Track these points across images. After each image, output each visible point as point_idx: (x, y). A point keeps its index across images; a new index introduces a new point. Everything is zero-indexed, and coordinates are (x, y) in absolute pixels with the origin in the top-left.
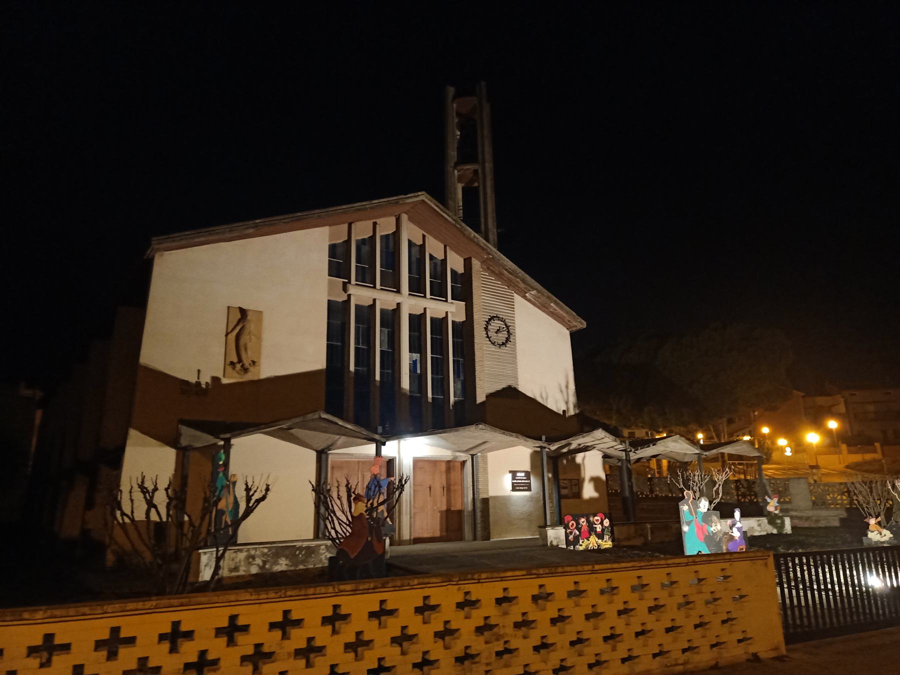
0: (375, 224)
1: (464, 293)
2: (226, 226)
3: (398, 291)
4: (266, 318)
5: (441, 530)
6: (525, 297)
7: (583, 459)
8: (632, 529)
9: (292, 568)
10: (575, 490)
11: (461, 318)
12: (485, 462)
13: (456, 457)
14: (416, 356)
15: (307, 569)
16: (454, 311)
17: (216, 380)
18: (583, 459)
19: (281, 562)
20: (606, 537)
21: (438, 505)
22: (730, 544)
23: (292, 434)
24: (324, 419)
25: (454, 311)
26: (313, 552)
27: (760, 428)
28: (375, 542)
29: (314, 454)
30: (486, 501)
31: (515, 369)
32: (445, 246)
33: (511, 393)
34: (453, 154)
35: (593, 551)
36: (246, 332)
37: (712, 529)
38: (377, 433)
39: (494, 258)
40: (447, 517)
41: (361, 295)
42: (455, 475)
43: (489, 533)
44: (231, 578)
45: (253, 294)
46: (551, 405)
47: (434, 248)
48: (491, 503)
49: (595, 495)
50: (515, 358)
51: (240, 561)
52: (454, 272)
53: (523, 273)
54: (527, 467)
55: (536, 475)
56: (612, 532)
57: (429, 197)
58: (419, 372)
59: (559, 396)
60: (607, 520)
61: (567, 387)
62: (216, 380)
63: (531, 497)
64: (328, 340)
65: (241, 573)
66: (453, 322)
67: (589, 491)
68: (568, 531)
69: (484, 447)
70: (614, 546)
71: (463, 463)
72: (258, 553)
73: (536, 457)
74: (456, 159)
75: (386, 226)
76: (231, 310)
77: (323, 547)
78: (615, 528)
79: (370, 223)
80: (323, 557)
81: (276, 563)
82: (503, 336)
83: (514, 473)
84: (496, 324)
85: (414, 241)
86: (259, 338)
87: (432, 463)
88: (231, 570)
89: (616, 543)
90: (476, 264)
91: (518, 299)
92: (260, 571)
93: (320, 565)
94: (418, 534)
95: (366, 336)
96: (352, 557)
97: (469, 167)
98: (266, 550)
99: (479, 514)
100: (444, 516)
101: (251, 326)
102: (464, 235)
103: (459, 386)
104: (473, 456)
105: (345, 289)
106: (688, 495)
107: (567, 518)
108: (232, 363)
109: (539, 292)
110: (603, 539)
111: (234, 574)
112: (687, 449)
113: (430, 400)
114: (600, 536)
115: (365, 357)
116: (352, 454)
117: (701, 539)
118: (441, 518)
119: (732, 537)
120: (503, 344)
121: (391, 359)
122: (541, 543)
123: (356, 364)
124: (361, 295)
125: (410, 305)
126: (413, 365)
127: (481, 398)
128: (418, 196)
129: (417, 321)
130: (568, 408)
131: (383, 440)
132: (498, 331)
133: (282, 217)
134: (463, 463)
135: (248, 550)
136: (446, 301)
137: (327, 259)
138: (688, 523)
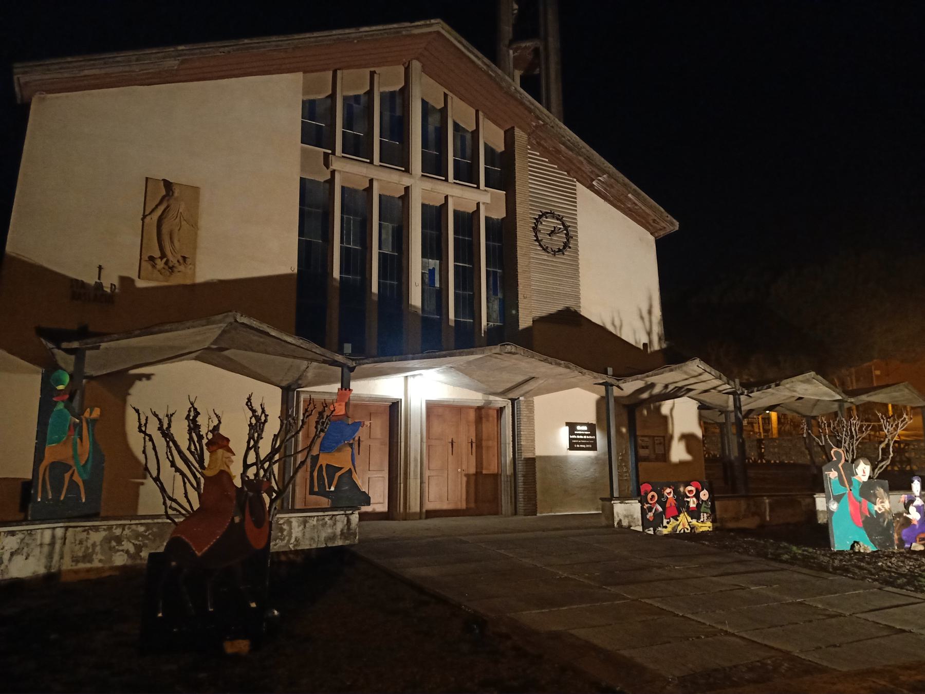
0: (372, 74)
1: (503, 176)
2: (131, 53)
3: (407, 171)
4: (205, 198)
6: (591, 187)
7: (672, 410)
8: (743, 504)
10: (660, 450)
11: (499, 214)
12: (531, 409)
13: (490, 402)
14: (434, 263)
16: (485, 201)
18: (672, 410)
20: (704, 516)
21: (464, 467)
22: (905, 531)
24: (243, 324)
25: (485, 201)
28: (249, 526)
29: (279, 391)
30: (531, 462)
31: (576, 286)
32: (477, 112)
33: (570, 318)
34: (507, 29)
35: (683, 536)
37: (876, 508)
38: (342, 354)
39: (545, 124)
41: (350, 172)
42: (488, 428)
43: (535, 505)
44: (76, 572)
46: (627, 335)
47: (461, 113)
48: (537, 464)
49: (687, 457)
50: (577, 270)
51: (94, 545)
52: (489, 151)
53: (588, 147)
54: (592, 419)
55: (602, 429)
56: (713, 509)
57: (447, 27)
58: (437, 285)
59: (638, 324)
60: (705, 491)
61: (650, 312)
63: (597, 459)
64: (301, 233)
65: (96, 564)
66: (487, 219)
67: (678, 453)
68: (646, 506)
69: (526, 388)
70: (715, 529)
71: (501, 410)
73: (602, 405)
74: (511, 36)
75: (389, 80)
76: (149, 181)
78: (716, 503)
79: (367, 71)
83: (572, 426)
84: (548, 224)
85: (431, 102)
87: (455, 410)
88: (76, 560)
89: (718, 525)
90: (520, 136)
91: (580, 188)
92: (129, 562)
94: (429, 506)
96: (199, 554)
97: (528, 44)
98: (141, 529)
99: (520, 479)
100: (473, 479)
102: (501, 88)
103: (496, 306)
104: (513, 401)
105: (327, 164)
107: (645, 487)
108: (151, 259)
109: (610, 176)
110: (698, 518)
111: (81, 566)
112: (826, 394)
113: (452, 324)
114: (695, 514)
115: (356, 261)
117: (857, 524)
118: (468, 483)
119: (908, 521)
121: (395, 266)
122: (603, 521)
125: (423, 190)
126: (428, 278)
127: (525, 322)
129: (434, 216)
130: (651, 341)
131: (351, 364)
132: (552, 233)
133: (218, 44)
134: (501, 410)
135: (110, 528)
136: (478, 188)
137: (300, 119)
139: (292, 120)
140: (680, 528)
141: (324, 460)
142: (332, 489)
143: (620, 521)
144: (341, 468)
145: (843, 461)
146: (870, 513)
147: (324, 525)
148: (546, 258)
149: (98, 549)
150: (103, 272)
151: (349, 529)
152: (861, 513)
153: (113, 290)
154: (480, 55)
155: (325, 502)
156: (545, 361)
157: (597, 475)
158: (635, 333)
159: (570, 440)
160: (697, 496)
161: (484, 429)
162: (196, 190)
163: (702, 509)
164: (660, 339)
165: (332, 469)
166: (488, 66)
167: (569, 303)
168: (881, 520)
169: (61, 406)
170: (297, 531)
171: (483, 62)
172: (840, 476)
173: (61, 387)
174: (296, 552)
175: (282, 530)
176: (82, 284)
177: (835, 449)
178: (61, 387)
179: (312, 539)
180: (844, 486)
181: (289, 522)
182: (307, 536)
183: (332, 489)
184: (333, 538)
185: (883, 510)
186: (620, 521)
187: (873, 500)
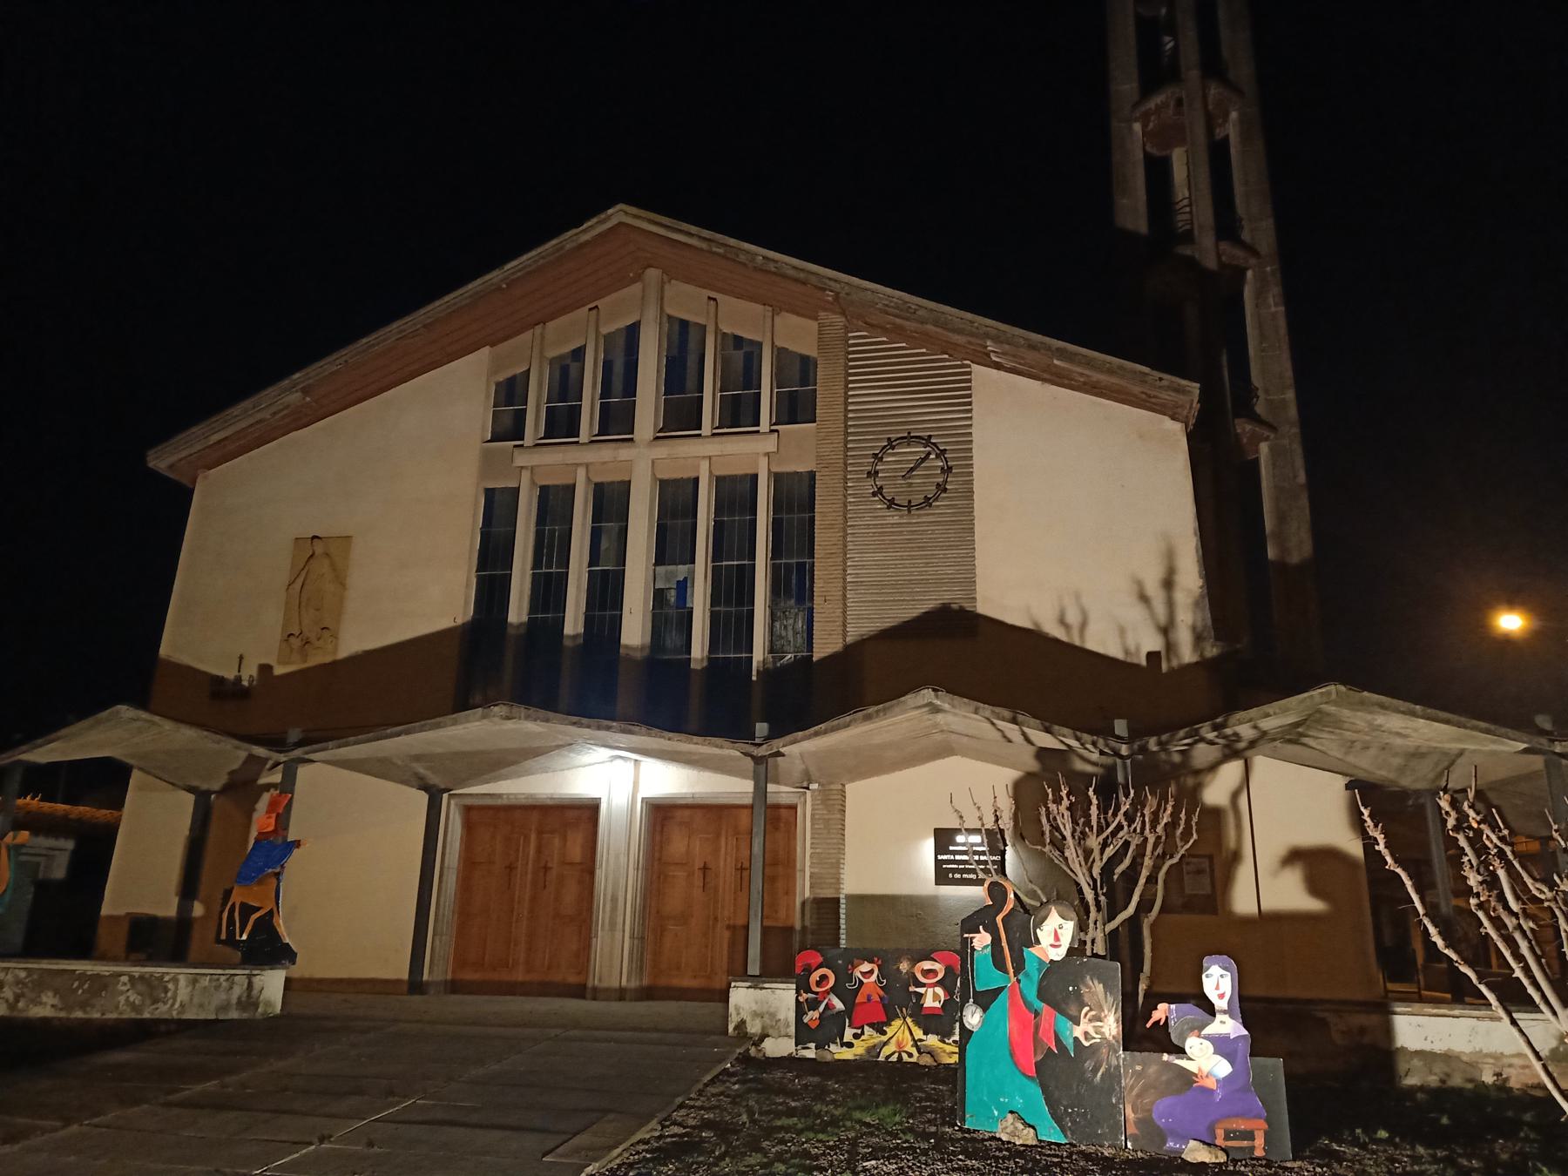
9: (62, 1014)
16: (757, 453)
17: (265, 669)
19: (44, 999)
23: (1013, 767)
26: (105, 987)
27: (1535, 624)
41: (538, 463)
46: (1101, 641)
50: (972, 531)
59: (1134, 614)
61: (1168, 584)
62: (265, 669)
77: (124, 979)
81: (37, 1002)
82: (923, 483)
83: (943, 838)
86: (341, 581)
93: (114, 1016)
95: (552, 547)
115: (549, 591)
116: (500, 796)
121: (606, 592)
128: (609, 218)
130: (1170, 646)
140: (886, 1051)
141: (237, 897)
142: (244, 937)
143: (743, 1022)
147: (217, 988)
148: (896, 520)
151: (249, 996)
152: (1037, 1041)
153: (251, 682)
154: (694, 229)
156: (580, 725)
159: (938, 863)
164: (1198, 638)
165: (247, 910)
168: (1089, 1065)
170: (183, 992)
172: (996, 942)
175: (166, 990)
176: (220, 680)
179: (201, 1006)
181: (175, 980)
183: (244, 937)
184: (225, 1007)
186: (743, 1022)
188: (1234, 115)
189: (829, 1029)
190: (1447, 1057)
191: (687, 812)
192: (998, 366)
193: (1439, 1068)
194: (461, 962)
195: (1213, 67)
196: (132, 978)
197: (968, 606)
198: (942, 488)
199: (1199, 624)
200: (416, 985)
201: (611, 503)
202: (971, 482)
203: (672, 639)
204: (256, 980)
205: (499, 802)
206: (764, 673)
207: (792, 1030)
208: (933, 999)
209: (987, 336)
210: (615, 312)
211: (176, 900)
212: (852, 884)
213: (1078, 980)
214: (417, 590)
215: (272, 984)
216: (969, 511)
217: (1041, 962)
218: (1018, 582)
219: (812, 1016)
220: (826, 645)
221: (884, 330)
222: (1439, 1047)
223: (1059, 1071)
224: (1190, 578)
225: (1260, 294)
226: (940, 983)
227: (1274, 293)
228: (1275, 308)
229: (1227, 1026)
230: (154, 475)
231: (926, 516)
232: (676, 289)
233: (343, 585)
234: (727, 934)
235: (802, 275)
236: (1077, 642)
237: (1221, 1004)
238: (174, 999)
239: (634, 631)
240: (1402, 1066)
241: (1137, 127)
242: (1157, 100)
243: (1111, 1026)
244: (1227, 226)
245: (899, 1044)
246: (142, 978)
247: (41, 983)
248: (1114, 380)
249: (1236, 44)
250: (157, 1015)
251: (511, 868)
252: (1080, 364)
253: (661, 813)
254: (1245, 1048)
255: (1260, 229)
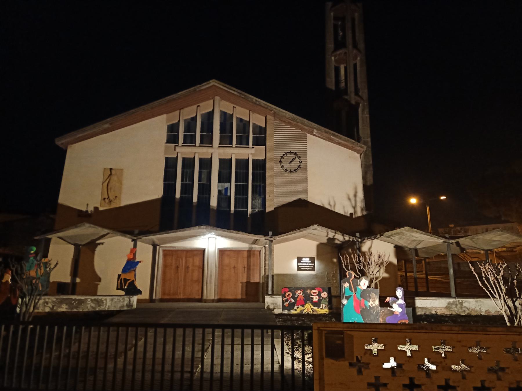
1: (261, 140)
5: (242, 294)
9: (69, 310)
15: (78, 312)
16: (251, 153)
17: (96, 208)
18: (370, 249)
19: (63, 306)
20: (323, 306)
34: (330, 45)
36: (111, 181)
37: (370, 304)
40: (247, 286)
41: (184, 152)
45: (123, 159)
46: (339, 210)
54: (314, 254)
56: (330, 303)
57: (217, 82)
59: (347, 203)
61: (355, 196)
62: (96, 208)
63: (316, 276)
64: (165, 180)
68: (284, 299)
70: (330, 313)
72: (50, 301)
75: (206, 107)
77: (89, 300)
79: (195, 106)
80: (89, 306)
81: (60, 307)
82: (295, 165)
83: (299, 259)
86: (120, 182)
91: (309, 136)
93: (87, 310)
95: (188, 176)
101: (114, 178)
106: (350, 275)
110: (318, 306)
112: (517, 240)
114: (317, 304)
115: (187, 189)
116: (175, 247)
120: (295, 170)
121: (205, 189)
123: (182, 193)
124: (184, 152)
129: (225, 164)
130: (355, 212)
135: (45, 299)
138: (347, 298)
139: (164, 135)
143: (269, 306)
144: (129, 280)
145: (353, 277)
146: (365, 306)
148: (287, 175)
149: (41, 306)
150: (89, 206)
154: (235, 89)
155: (123, 293)
157: (316, 284)
158: (344, 207)
159: (298, 266)
160: (319, 295)
161: (252, 260)
162: (122, 170)
163: (322, 302)
164: (362, 210)
165: (126, 280)
166: (240, 93)
167: (302, 197)
169: (32, 258)
170: (109, 303)
171: (239, 93)
172: (350, 286)
173: (32, 252)
174: (108, 311)
175: (103, 303)
177: (348, 272)
178: (32, 252)
179: (115, 307)
180: (352, 291)
181: (106, 300)
182: (113, 305)
183: (126, 288)
184: (123, 306)
185: (374, 305)
186: (269, 306)
187: (368, 299)
188: (359, 58)
189: (291, 306)
190: (426, 308)
191: (229, 252)
192: (314, 135)
193: (424, 311)
194: (164, 293)
195: (355, 46)
196: (91, 300)
197: (306, 199)
198: (299, 167)
199: (362, 206)
200: (151, 300)
201: (206, 164)
202: (306, 166)
203: (224, 204)
204: (131, 299)
205: (175, 249)
206: (252, 215)
207: (281, 307)
208: (315, 299)
209: (315, 128)
210: (206, 107)
211: (70, 277)
212: (276, 272)
213: (370, 293)
214: (145, 186)
215: (134, 299)
216: (306, 174)
217: (361, 289)
218: (318, 195)
219: (286, 304)
220: (269, 208)
221: (284, 122)
222: (424, 306)
223: (364, 311)
224: (361, 195)
225: (363, 110)
226: (317, 295)
227: (367, 111)
228: (367, 115)
229: (401, 302)
230: (57, 147)
231: (294, 174)
232: (224, 103)
233: (121, 184)
234: (241, 284)
235: (266, 106)
236: (333, 210)
237: (400, 297)
238: (106, 304)
239: (214, 202)
240: (417, 310)
241: (333, 58)
242: (338, 52)
243: (377, 302)
244: (357, 93)
245: (308, 309)
246: (95, 300)
247: (61, 302)
248: (346, 143)
249: (360, 37)
250: (101, 309)
251: (177, 267)
252: (338, 138)
253: (222, 252)
254: (405, 306)
255: (364, 93)
